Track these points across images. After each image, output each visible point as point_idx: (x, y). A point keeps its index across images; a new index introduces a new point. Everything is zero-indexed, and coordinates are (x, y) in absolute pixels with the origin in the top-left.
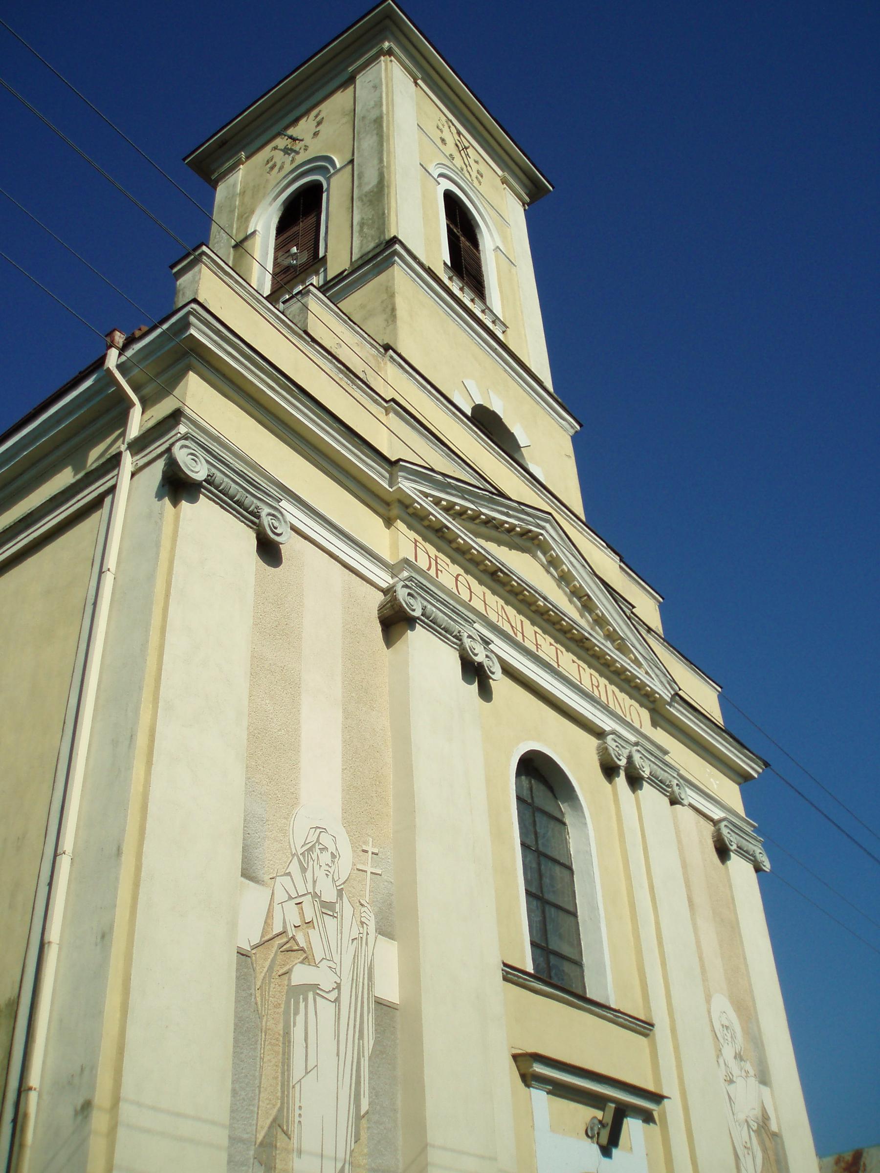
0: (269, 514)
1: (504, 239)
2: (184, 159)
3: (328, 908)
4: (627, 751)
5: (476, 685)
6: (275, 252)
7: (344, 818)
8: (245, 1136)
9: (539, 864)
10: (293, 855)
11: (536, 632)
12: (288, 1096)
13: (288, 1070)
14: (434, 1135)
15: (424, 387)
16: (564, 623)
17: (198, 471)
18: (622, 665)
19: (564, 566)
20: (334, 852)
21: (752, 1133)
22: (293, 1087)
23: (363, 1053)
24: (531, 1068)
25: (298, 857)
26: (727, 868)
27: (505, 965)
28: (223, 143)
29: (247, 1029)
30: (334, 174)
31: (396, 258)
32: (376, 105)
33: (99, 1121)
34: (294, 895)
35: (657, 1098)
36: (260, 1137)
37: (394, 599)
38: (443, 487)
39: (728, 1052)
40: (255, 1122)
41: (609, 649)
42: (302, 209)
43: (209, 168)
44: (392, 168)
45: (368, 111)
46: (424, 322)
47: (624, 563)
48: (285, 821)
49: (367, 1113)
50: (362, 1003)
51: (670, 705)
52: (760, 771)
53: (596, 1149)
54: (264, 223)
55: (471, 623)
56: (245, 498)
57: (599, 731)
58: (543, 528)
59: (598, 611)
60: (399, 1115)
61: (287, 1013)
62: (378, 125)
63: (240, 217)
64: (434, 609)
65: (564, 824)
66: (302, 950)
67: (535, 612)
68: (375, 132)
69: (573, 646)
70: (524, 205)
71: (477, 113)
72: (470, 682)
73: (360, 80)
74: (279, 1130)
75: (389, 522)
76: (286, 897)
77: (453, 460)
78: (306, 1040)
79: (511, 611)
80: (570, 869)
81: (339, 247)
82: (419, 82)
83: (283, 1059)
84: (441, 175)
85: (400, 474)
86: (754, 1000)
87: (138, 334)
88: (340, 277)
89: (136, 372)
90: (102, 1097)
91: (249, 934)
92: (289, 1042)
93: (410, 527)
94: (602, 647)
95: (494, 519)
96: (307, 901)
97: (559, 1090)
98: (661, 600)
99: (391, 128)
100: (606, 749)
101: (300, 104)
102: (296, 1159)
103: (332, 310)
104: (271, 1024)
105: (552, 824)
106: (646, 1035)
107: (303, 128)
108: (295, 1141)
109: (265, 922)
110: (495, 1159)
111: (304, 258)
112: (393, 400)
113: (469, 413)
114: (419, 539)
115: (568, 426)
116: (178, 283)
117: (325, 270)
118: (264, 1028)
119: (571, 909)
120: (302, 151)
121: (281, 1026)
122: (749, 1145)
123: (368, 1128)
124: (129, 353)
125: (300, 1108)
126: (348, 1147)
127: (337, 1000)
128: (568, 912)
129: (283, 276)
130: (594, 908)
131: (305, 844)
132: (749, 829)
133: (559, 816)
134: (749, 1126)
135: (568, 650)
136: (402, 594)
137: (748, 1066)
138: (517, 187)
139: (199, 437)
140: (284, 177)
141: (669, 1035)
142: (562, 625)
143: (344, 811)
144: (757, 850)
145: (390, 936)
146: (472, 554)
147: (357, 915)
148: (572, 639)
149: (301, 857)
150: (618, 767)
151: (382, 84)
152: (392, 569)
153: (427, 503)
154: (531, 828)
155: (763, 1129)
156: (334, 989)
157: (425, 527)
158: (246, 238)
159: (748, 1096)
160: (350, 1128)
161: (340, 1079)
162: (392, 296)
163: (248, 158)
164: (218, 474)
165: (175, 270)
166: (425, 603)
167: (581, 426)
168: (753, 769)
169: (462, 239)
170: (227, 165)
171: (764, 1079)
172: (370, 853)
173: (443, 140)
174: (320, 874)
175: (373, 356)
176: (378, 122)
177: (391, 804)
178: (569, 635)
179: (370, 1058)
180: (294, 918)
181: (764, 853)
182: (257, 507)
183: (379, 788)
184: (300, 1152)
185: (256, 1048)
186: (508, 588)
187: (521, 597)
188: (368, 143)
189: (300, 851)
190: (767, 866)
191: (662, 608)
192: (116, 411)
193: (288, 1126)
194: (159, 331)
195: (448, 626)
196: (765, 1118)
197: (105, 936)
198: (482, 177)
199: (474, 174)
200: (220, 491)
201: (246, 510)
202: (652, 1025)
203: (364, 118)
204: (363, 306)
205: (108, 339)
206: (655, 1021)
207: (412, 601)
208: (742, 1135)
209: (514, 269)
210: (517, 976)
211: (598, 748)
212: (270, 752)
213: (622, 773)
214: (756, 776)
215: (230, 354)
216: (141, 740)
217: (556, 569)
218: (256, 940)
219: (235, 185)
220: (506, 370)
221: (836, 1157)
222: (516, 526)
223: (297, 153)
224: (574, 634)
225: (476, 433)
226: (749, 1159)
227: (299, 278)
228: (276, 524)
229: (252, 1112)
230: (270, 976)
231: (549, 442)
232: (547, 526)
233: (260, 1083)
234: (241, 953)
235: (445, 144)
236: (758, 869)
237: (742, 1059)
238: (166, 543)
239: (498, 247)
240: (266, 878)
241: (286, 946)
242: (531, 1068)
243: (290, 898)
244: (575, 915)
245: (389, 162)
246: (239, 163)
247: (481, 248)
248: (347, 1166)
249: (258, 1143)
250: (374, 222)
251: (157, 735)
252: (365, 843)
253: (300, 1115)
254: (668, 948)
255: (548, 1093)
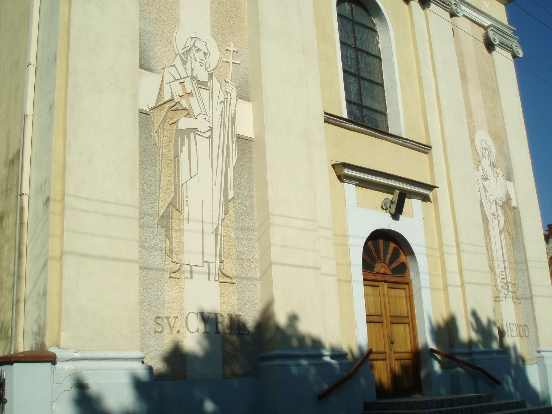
3: (202, 84)
21: (499, 208)
23: (229, 166)
24: (343, 171)
25: (180, 55)
26: (492, 56)
27: (326, 113)
36: (161, 213)
39: (485, 163)
40: (157, 205)
48: (169, 34)
49: (233, 198)
53: (388, 216)
61: (176, 144)
65: (376, 31)
66: (185, 109)
76: (173, 79)
78: (190, 159)
80: (379, 58)
83: (175, 171)
90: (55, 194)
91: (148, 101)
92: (178, 161)
96: (187, 82)
97: (362, 183)
104: (165, 152)
106: (427, 153)
118: (161, 154)
119: (380, 82)
122: (495, 214)
125: (187, 196)
126: (221, 216)
127: (210, 137)
130: (393, 80)
131: (185, 48)
132: (510, 32)
134: (496, 203)
137: (499, 170)
143: (212, 27)
145: (248, 99)
147: (223, 88)
149: (182, 56)
155: (507, 205)
159: (497, 188)
160: (221, 208)
161: (214, 180)
171: (509, 178)
174: (196, 65)
179: (234, 169)
180: (178, 90)
181: (519, 46)
184: (188, 220)
189: (181, 52)
190: (521, 54)
193: (179, 207)
196: (508, 199)
202: (431, 147)
218: (153, 104)
226: (495, 221)
230: (164, 125)
233: (160, 184)
236: (515, 56)
237: (494, 167)
240: (158, 69)
242: (343, 171)
243: (175, 80)
244: (382, 85)
248: (220, 227)
249: (160, 215)
253: (187, 201)
255: (356, 185)
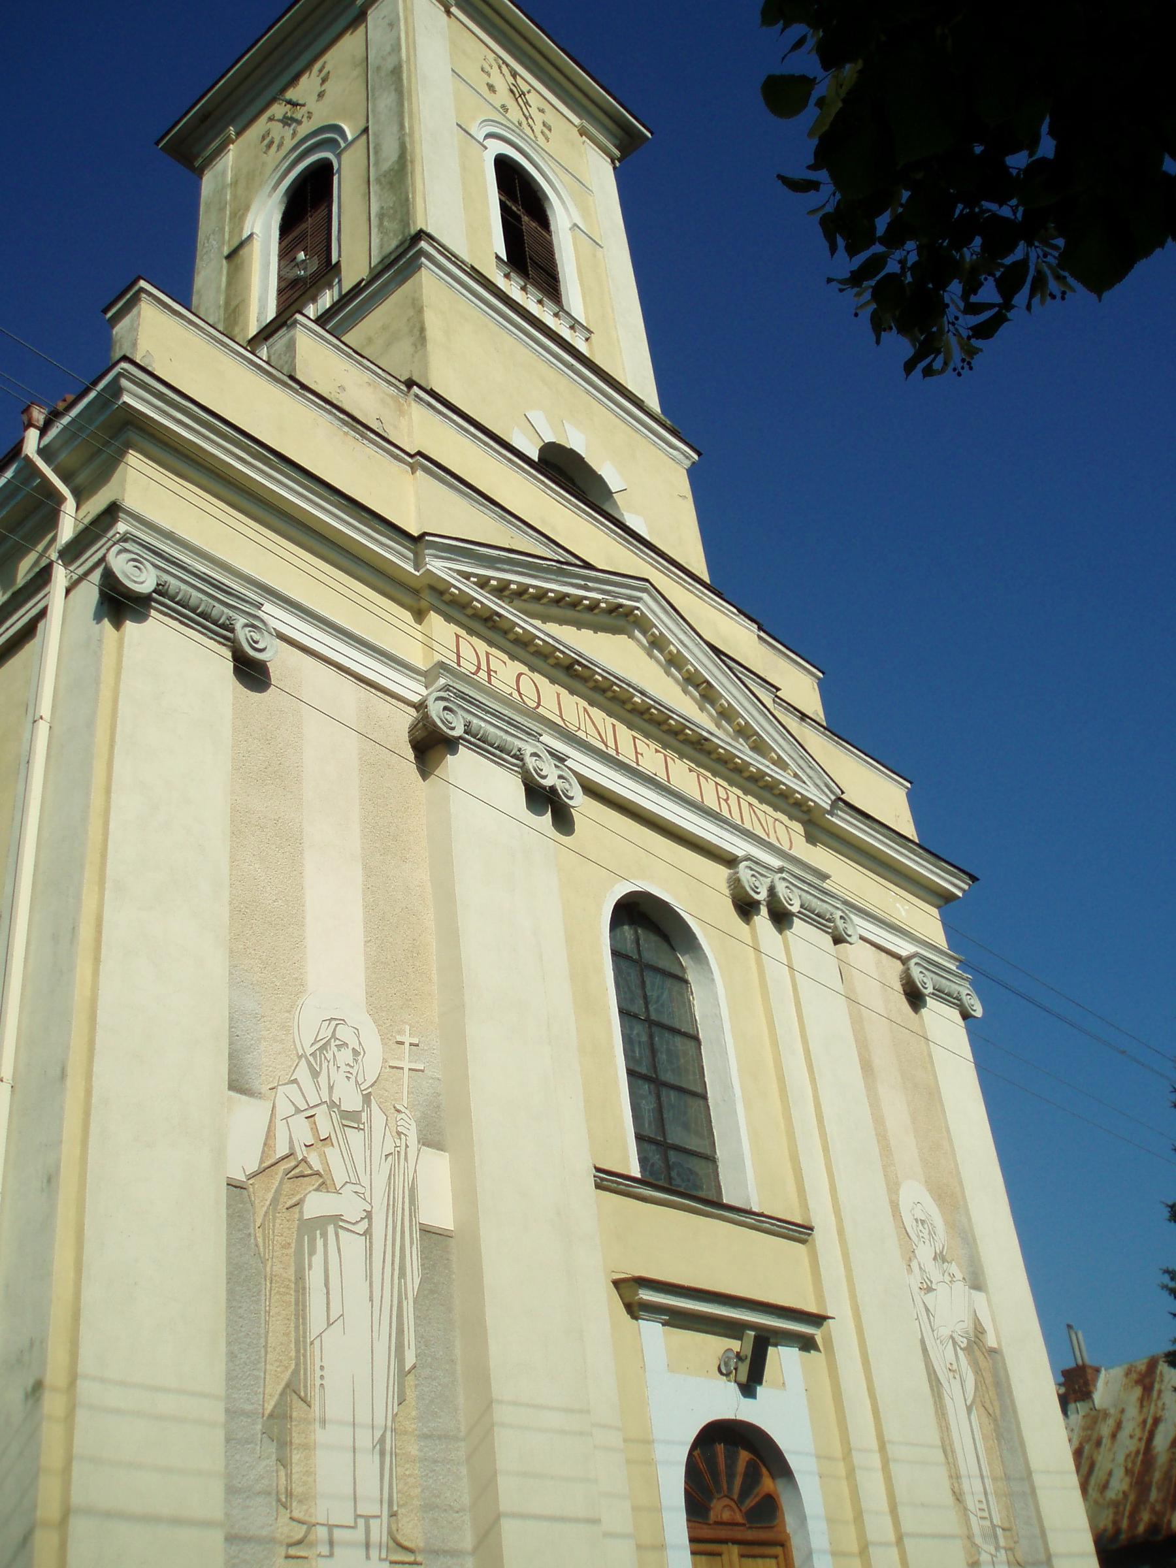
0: (246, 625)
1: (585, 211)
2: (157, 143)
3: (350, 1118)
4: (769, 880)
5: (548, 816)
6: (279, 260)
7: (369, 1004)
8: (248, 1407)
9: (651, 1037)
10: (300, 1057)
11: (634, 738)
12: (305, 1356)
13: (304, 1324)
14: (501, 1388)
15: (466, 431)
16: (672, 722)
17: (143, 581)
18: (758, 769)
19: (672, 647)
20: (357, 1048)
22: (312, 1343)
23: (406, 1294)
24: (638, 1296)
26: (921, 1017)
27: (598, 1170)
28: (204, 117)
29: (244, 1278)
30: (345, 148)
31: (423, 259)
32: (393, 50)
33: (53, 1404)
34: (303, 1106)
35: (818, 1320)
36: (269, 1408)
37: (426, 717)
38: (490, 562)
39: (925, 1253)
40: (261, 1390)
41: (743, 751)
42: (309, 199)
43: (191, 152)
44: (417, 136)
45: (384, 58)
46: (466, 342)
47: (765, 632)
49: (414, 1367)
50: (403, 1232)
51: (831, 813)
52: (966, 887)
53: (733, 1388)
54: (264, 221)
55: (536, 736)
56: (212, 610)
57: (732, 857)
58: (638, 599)
59: (723, 701)
60: (458, 1367)
62: (396, 77)
63: (234, 215)
64: (483, 724)
65: (686, 982)
66: (318, 1174)
67: (631, 711)
68: (393, 87)
69: (688, 750)
70: (613, 162)
71: (539, 44)
72: (540, 813)
73: (373, 15)
74: (295, 1397)
75: (419, 616)
77: (510, 522)
78: (327, 1285)
79: (596, 713)
80: (696, 1039)
81: (356, 249)
82: (454, 10)
83: (297, 1310)
84: (490, 135)
85: (427, 551)
86: (961, 1183)
87: (61, 406)
88: (357, 289)
89: (62, 457)
90: (55, 1375)
91: (243, 1160)
92: (304, 1288)
93: (449, 619)
94: (728, 748)
95: (568, 595)
96: (321, 1114)
98: (821, 675)
99: (413, 80)
100: (738, 880)
101: (300, 53)
102: (319, 1431)
103: (330, 343)
104: (278, 1269)
105: (669, 982)
106: (803, 1242)
107: (305, 88)
108: (317, 1409)
109: (265, 1144)
110: (588, 1412)
111: (313, 266)
112: (419, 453)
113: (535, 456)
114: (462, 633)
115: (681, 457)
116: (115, 331)
117: (340, 281)
119: (699, 1090)
120: (305, 120)
121: (292, 1271)
122: (955, 1367)
123: (416, 1386)
124: (53, 432)
125: (322, 1368)
127: (368, 1233)
128: (694, 1094)
129: (291, 292)
130: (727, 1087)
131: (316, 1042)
133: (675, 970)
134: (955, 1343)
135: (682, 756)
136: (435, 710)
137: (953, 1268)
138: (601, 138)
139: (143, 537)
140: (285, 158)
141: (836, 1236)
142: (670, 725)
143: (369, 995)
144: (964, 990)
145: (439, 1146)
146: (537, 645)
147: (392, 1124)
148: (687, 741)
149: (311, 1059)
150: (758, 903)
151: (399, 19)
152: (428, 676)
153: (467, 586)
154: (639, 991)
155: (978, 1346)
156: (362, 1219)
157: (468, 616)
158: (242, 244)
159: (952, 1308)
160: (391, 1388)
162: (420, 311)
163: (239, 134)
164: (173, 582)
165: (109, 315)
166: (469, 718)
167: (699, 454)
168: (955, 886)
169: (525, 219)
170: (214, 145)
171: (976, 1283)
172: (407, 1045)
173: (491, 88)
174: (338, 1077)
175: (392, 397)
176: (397, 71)
177: (435, 978)
178: (681, 737)
180: (303, 1133)
181: (974, 994)
182: (229, 618)
183: (413, 962)
184: (323, 1422)
185: (259, 1300)
186: (591, 684)
187: (610, 694)
188: (385, 101)
189: (309, 1051)
191: (823, 687)
192: (46, 509)
194: (92, 395)
195: (503, 744)
196: (979, 1331)
197: (51, 1180)
198: (550, 130)
199: (538, 127)
200: (177, 603)
201: (215, 623)
202: (811, 1229)
203: (378, 68)
204: (385, 328)
205: (25, 418)
206: (815, 1222)
207: (449, 717)
208: (944, 1355)
209: (599, 252)
210: (612, 1181)
211: (729, 880)
212: (262, 933)
213: (764, 910)
214: (960, 894)
215: (179, 422)
216: (86, 932)
217: (661, 651)
218: (253, 1167)
219: (224, 173)
220: (588, 392)
221: (1126, 1366)
222: (599, 601)
223: (299, 122)
224: (687, 734)
225: (542, 482)
226: (956, 1385)
227: (309, 294)
228: (256, 637)
229: (257, 1377)
230: (275, 1209)
231: (655, 483)
232: (645, 596)
233: (266, 1342)
234: (232, 1185)
235: (494, 92)
236: (966, 1016)
237: (944, 1260)
238: (107, 677)
239: (575, 225)
240: (264, 1089)
241: (295, 1171)
242: (638, 1296)
243: (298, 1111)
244: (704, 1097)
245: (411, 128)
246: (227, 142)
247: (552, 228)
248: (388, 1433)
250: (396, 212)
251: (105, 923)
252: (400, 1032)
254: (831, 1129)
255: (664, 1325)
